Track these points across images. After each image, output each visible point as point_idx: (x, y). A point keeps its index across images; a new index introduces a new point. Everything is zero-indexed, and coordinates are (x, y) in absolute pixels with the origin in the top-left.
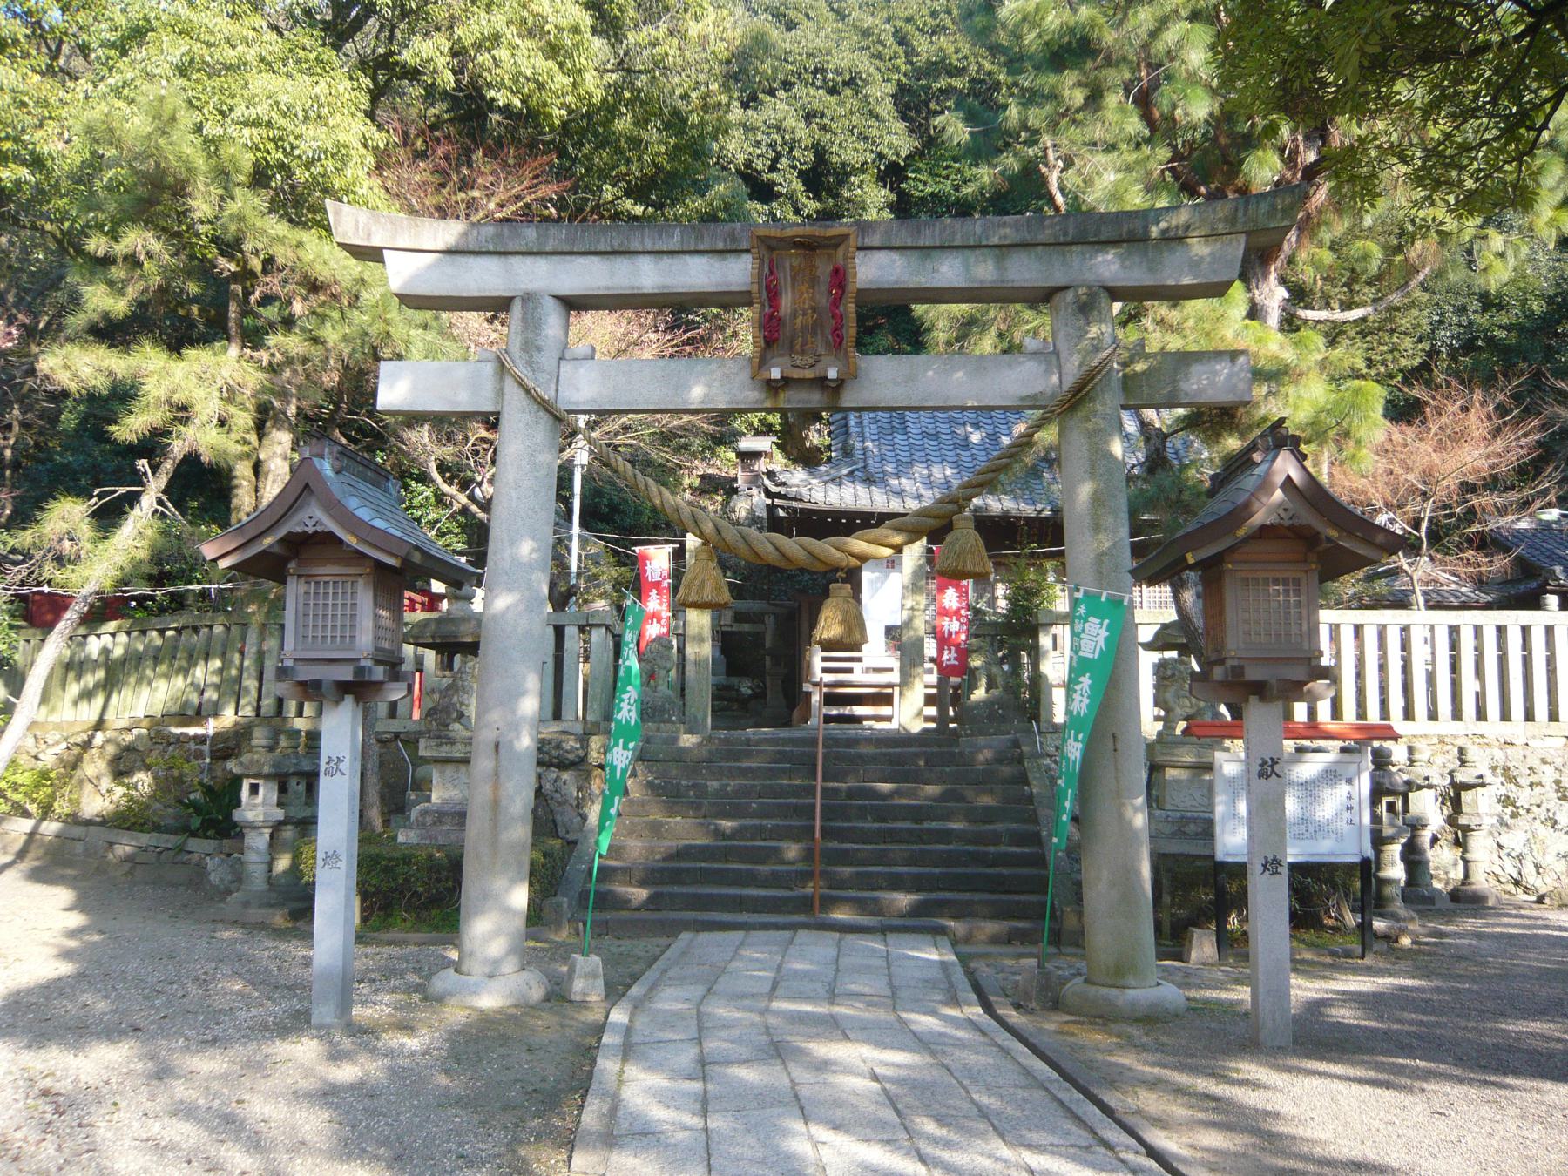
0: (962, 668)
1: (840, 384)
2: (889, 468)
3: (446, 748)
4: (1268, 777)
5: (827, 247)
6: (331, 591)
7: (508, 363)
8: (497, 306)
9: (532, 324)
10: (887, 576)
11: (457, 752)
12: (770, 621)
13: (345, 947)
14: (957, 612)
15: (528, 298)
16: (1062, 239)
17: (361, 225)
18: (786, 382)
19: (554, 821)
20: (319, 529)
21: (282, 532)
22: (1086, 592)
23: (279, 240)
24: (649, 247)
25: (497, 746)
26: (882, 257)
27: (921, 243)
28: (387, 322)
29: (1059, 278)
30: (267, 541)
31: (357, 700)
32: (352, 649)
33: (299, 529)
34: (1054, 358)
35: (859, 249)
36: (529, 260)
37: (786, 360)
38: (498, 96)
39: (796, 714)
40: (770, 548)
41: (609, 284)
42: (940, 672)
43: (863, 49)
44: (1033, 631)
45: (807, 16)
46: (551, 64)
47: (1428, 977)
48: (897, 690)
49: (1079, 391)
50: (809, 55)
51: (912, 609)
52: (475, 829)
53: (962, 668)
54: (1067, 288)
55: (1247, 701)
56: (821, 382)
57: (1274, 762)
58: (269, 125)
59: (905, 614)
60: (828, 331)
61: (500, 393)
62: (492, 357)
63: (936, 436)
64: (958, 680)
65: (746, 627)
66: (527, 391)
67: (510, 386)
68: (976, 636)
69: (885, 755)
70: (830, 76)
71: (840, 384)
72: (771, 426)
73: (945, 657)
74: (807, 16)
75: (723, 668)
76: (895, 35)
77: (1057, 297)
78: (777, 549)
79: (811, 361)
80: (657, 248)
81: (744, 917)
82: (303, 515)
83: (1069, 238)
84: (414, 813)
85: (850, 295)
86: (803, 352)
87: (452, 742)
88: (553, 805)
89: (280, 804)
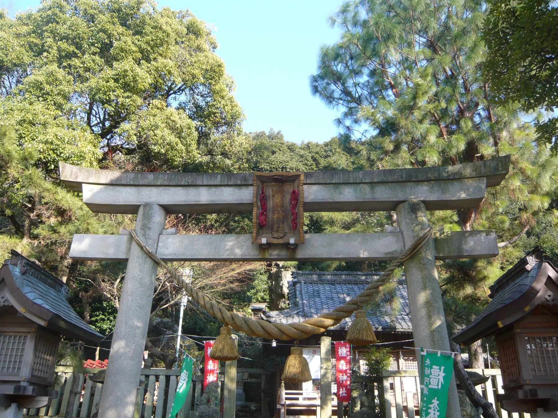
0: (349, 397)
1: (296, 246)
2: (313, 311)
5: (289, 181)
7: (134, 235)
8: (133, 209)
9: (148, 217)
10: (313, 357)
12: (264, 377)
14: (345, 371)
16: (400, 180)
17: (74, 172)
18: (269, 246)
20: (6, 304)
22: (427, 351)
23: (48, 190)
24: (205, 183)
26: (315, 188)
27: (334, 182)
28: (88, 224)
29: (399, 197)
32: (17, 375)
34: (400, 234)
35: (305, 184)
36: (149, 188)
37: (270, 235)
38: (155, 148)
40: (260, 328)
41: (186, 199)
42: (338, 399)
43: (300, 162)
44: (380, 380)
45: (279, 149)
46: (177, 139)
48: (319, 408)
49: (414, 249)
50: (281, 163)
51: (326, 369)
53: (349, 397)
56: (286, 245)
58: (52, 143)
59: (323, 371)
60: (290, 222)
61: (129, 249)
62: (127, 233)
63: (332, 299)
64: (347, 403)
65: (253, 380)
66: (142, 248)
67: (134, 246)
68: (354, 382)
70: (288, 170)
71: (296, 246)
72: (266, 299)
73: (341, 392)
74: (279, 149)
75: (244, 398)
76: (312, 157)
77: (400, 206)
78: (263, 328)
79: (282, 235)
80: (209, 184)
83: (404, 179)
86: (278, 231)
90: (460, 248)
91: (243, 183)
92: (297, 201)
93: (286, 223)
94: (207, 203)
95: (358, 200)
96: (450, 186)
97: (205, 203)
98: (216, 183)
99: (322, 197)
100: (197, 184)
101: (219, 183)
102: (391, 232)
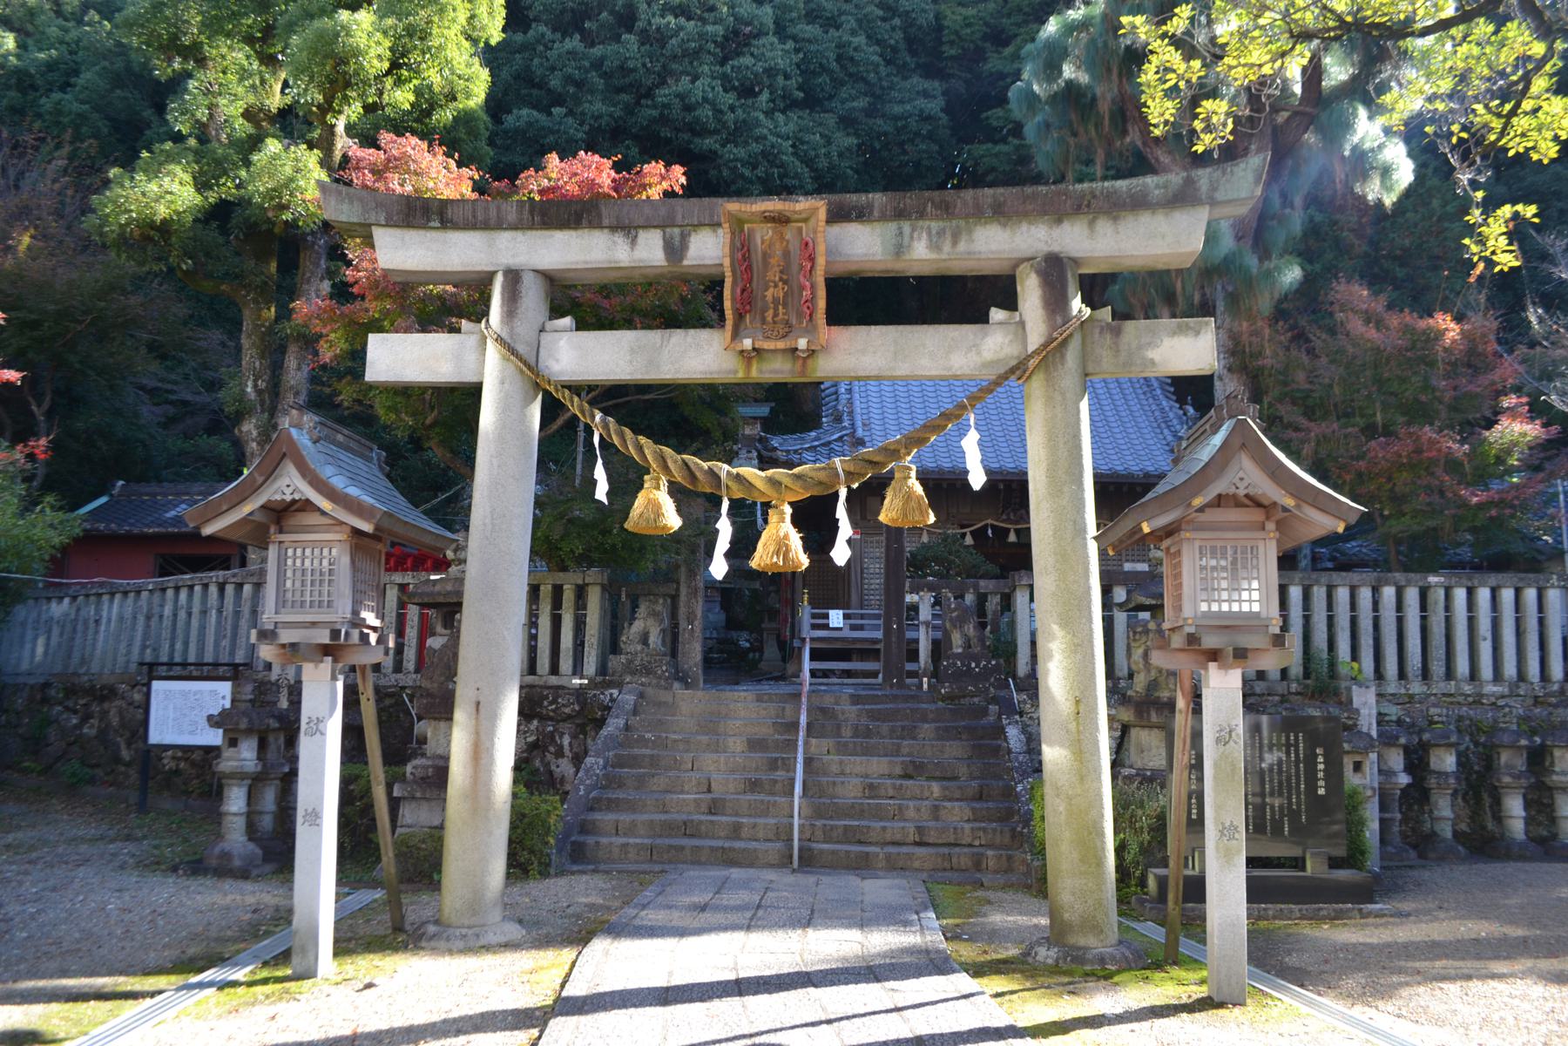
20: (297, 497)
25: (478, 704)
33: (278, 497)
47: (1531, 925)
55: (1206, 669)
82: (282, 482)
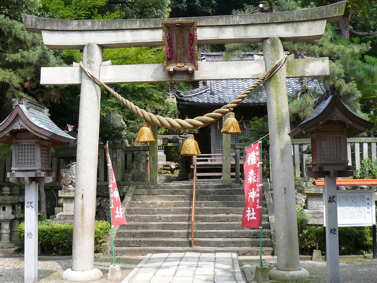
3: (67, 193)
4: (332, 202)
6: (26, 148)
11: (71, 195)
13: (37, 223)
15: (89, 45)
16: (265, 22)
18: (175, 72)
19: (105, 216)
20: (22, 128)
21: (10, 130)
30: (6, 132)
31: (36, 183)
33: (15, 128)
35: (198, 26)
39: (189, 175)
52: (78, 218)
54: (267, 38)
57: (334, 197)
69: (217, 191)
80: (131, 28)
81: (169, 248)
83: (268, 22)
84: (58, 215)
85: (195, 43)
87: (69, 191)
88: (105, 210)
89: (13, 213)
90: (303, 71)
91: (155, 27)
92: (193, 41)
93: (186, 56)
94: (131, 42)
95: (236, 38)
96: (300, 26)
97: (130, 42)
98: (136, 27)
99: (210, 36)
100: (123, 28)
101: (138, 27)
102: (257, 60)
